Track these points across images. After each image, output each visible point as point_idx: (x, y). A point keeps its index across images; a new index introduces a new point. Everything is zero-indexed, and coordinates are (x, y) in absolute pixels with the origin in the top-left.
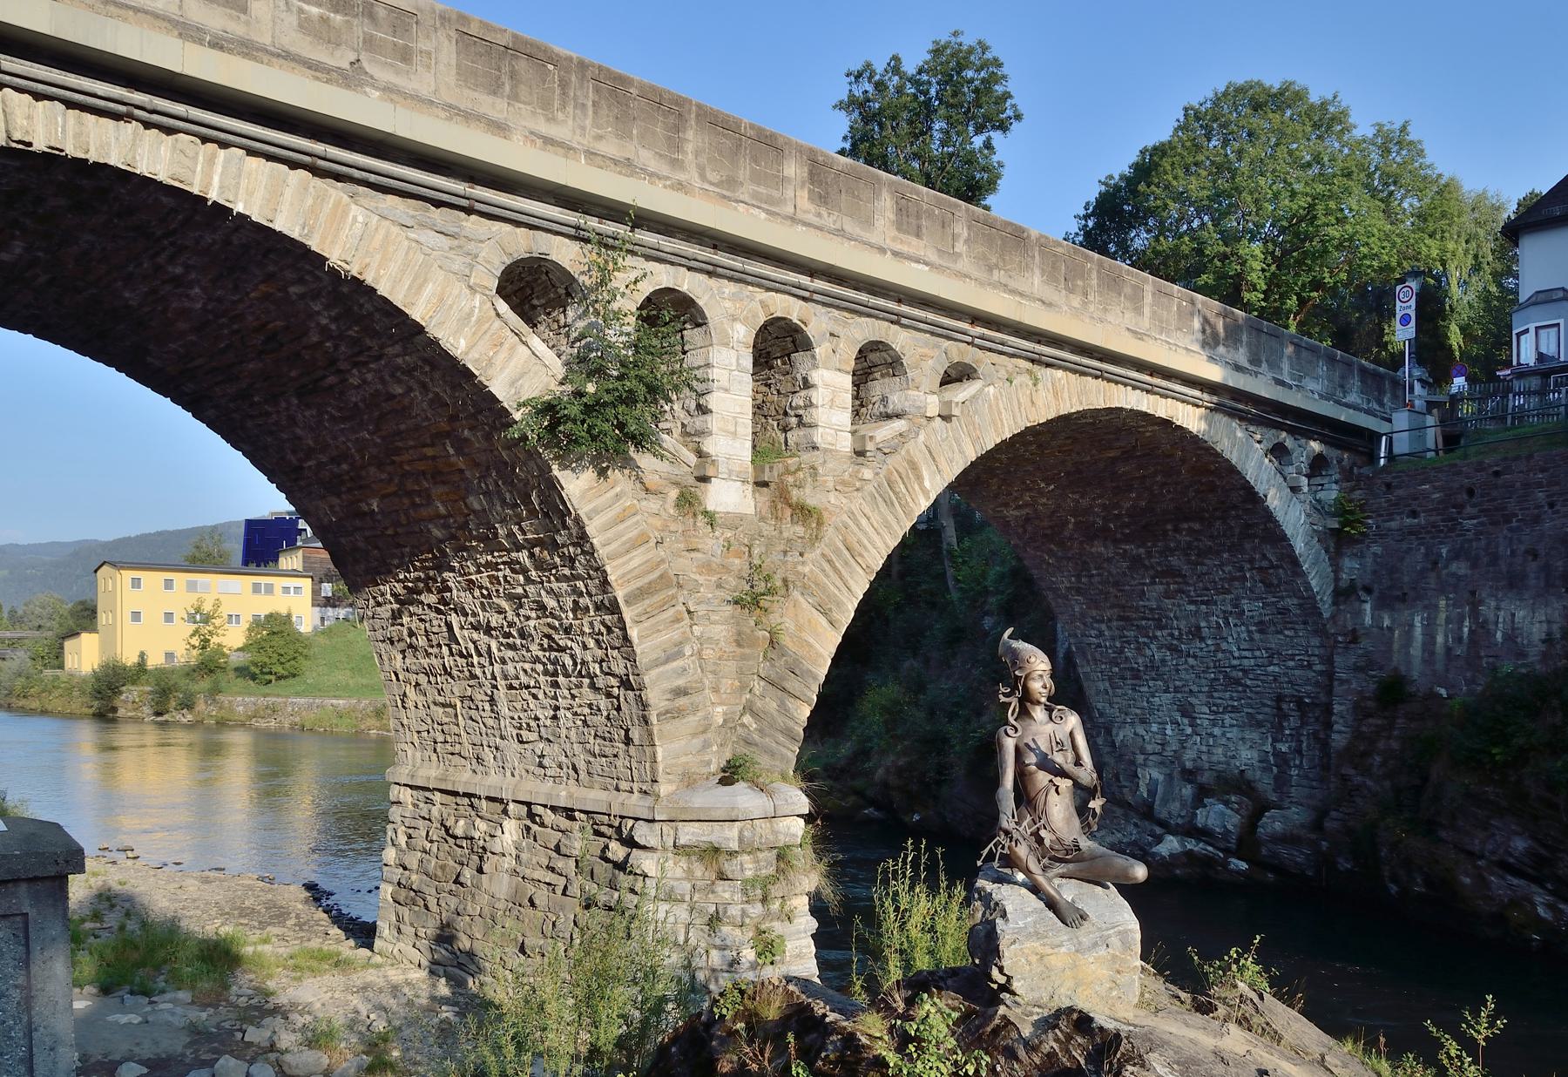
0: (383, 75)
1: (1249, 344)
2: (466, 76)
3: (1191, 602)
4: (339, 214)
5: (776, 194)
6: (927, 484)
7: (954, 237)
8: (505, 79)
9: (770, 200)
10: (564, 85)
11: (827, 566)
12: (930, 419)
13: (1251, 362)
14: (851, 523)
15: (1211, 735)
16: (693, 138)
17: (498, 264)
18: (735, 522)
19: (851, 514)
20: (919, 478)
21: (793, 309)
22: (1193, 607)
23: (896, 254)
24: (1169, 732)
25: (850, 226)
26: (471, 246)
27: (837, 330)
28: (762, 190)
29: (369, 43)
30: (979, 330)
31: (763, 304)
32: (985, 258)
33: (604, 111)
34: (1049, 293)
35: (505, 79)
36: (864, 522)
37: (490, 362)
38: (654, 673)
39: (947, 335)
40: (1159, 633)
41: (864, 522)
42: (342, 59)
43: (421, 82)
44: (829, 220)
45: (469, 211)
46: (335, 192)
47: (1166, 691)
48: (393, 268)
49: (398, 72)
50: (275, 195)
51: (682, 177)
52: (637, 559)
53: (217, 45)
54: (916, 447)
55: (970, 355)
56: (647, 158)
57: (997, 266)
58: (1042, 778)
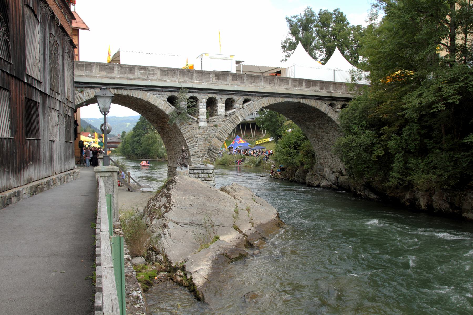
0: (150, 77)
1: (320, 86)
4: (146, 95)
5: (209, 80)
6: (240, 119)
7: (244, 80)
8: (167, 74)
9: (208, 81)
10: (175, 73)
11: (220, 133)
12: (240, 109)
13: (321, 89)
15: (336, 161)
17: (167, 97)
18: (204, 128)
19: (225, 125)
20: (238, 118)
21: (213, 96)
23: (231, 85)
25: (222, 82)
26: (163, 95)
27: (222, 97)
28: (207, 80)
29: (149, 74)
30: (250, 93)
31: (208, 96)
32: (251, 82)
33: (181, 75)
34: (265, 85)
35: (167, 74)
36: (227, 126)
37: (166, 110)
38: (191, 149)
39: (225, 94)
41: (227, 126)
42: (146, 77)
43: (155, 77)
45: (163, 91)
46: (146, 92)
48: (153, 100)
49: (152, 77)
50: (138, 95)
52: (188, 134)
53: (131, 79)
54: (237, 114)
55: (248, 97)
56: (188, 80)
57: (253, 83)
58: (72, 101)
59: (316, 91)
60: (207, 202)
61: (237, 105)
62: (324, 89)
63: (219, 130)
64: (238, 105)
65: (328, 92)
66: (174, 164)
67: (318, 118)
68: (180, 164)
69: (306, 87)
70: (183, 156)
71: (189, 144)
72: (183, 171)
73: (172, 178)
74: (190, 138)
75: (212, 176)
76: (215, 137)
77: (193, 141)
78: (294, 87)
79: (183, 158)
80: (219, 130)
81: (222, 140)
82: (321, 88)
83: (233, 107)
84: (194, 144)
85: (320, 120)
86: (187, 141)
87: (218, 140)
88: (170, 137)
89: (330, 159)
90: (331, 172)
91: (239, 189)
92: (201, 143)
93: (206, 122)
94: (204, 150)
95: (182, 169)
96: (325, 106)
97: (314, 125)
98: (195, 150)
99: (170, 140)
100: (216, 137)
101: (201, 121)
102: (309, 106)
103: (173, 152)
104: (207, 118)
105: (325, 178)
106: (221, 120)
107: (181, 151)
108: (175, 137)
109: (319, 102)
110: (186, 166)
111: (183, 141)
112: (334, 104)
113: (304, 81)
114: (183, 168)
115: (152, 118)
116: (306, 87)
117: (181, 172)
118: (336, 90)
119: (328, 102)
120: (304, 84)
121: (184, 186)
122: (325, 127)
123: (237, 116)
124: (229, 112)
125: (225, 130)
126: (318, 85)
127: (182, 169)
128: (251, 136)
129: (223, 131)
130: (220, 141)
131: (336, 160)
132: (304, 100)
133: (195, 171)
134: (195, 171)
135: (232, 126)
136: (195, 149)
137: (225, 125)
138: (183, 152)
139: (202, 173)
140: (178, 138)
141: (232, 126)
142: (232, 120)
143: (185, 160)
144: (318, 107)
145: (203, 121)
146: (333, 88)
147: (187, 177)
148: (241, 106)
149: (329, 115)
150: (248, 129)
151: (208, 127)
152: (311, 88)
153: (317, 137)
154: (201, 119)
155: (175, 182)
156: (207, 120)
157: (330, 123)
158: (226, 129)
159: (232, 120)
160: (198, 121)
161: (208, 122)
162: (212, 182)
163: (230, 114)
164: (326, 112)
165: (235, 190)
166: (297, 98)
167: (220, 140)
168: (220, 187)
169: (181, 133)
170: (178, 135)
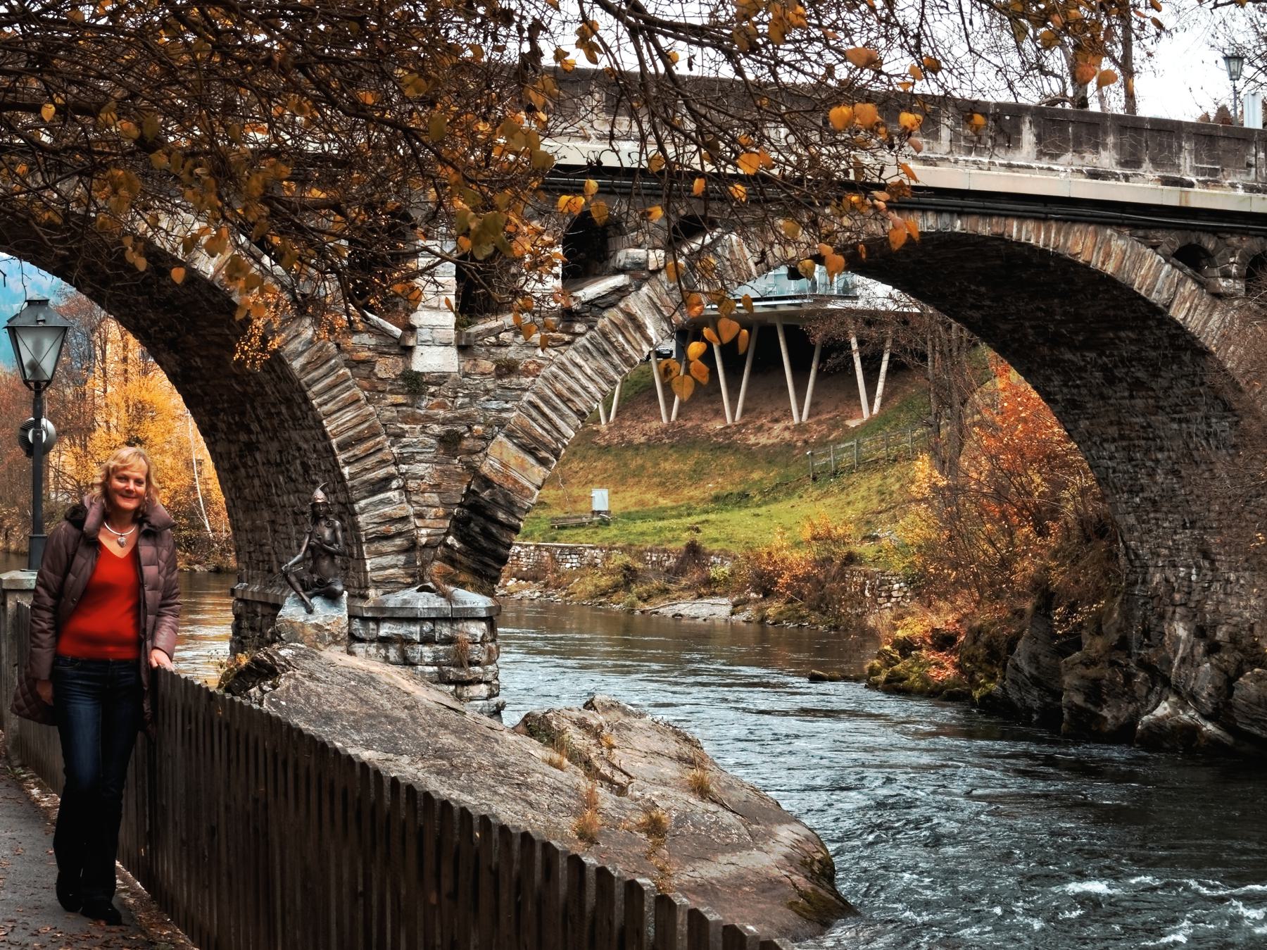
1: (1119, 147)
3: (1173, 420)
11: (534, 413)
13: (1123, 164)
14: (561, 374)
15: (1228, 581)
19: (562, 367)
20: (640, 328)
22: (1175, 426)
24: (1194, 578)
40: (1160, 456)
47: (1184, 527)
52: (348, 415)
59: (1094, 175)
60: (433, 777)
61: (632, 251)
62: (1147, 165)
63: (528, 396)
64: (639, 253)
65: (1166, 181)
66: (271, 584)
67: (1124, 329)
68: (302, 582)
69: (1041, 154)
70: (315, 541)
71: (353, 476)
72: (313, 620)
73: (261, 655)
74: (360, 440)
75: (484, 658)
76: (501, 437)
77: (379, 456)
78: (969, 152)
79: (318, 552)
80: (528, 396)
81: (543, 454)
82: (1131, 161)
83: (612, 264)
84: (381, 473)
85: (1132, 341)
86: (341, 457)
87: (522, 455)
88: (250, 432)
89: (1199, 568)
90: (1200, 649)
91: (619, 728)
92: (419, 469)
93: (453, 351)
94: (441, 512)
95: (310, 611)
96: (1153, 259)
97: (1104, 368)
98: (387, 510)
99: (251, 447)
100: (510, 435)
101: (424, 343)
102: (1058, 257)
103: (266, 515)
104: (458, 325)
105: (1166, 682)
106: (536, 338)
107: (307, 509)
108: (275, 430)
109: (1119, 244)
110: (332, 598)
111: (320, 457)
112: (1205, 251)
113: (1027, 119)
114: (317, 603)
115: (154, 322)
116: (1041, 154)
117: (303, 625)
118: (1214, 172)
119: (1172, 240)
120: (1028, 136)
121: (318, 695)
122: (1165, 384)
123: (632, 317)
124: (592, 290)
125: (559, 396)
126: (1111, 140)
127: (310, 611)
128: (787, 412)
129: (547, 401)
130: (531, 460)
131: (1232, 577)
132: (1030, 225)
133: (385, 630)
134: (385, 630)
135: (601, 373)
136: (389, 502)
137: (562, 367)
138: (316, 519)
139: (427, 640)
140: (295, 435)
141: (601, 373)
142: (605, 335)
143: (325, 563)
144: (1110, 269)
145: (432, 343)
146: (1198, 159)
147: (335, 655)
148: (656, 257)
149: (1178, 313)
150: (767, 365)
151: (466, 375)
152: (1068, 157)
153: (1122, 437)
154: (424, 334)
155: (277, 674)
156: (459, 336)
157: (1187, 357)
158: (570, 389)
159: (605, 335)
160: (411, 342)
161: (464, 349)
162: (483, 689)
163: (591, 303)
165: (595, 733)
166: (986, 214)
167: (531, 452)
168: (517, 719)
169: (312, 408)
170: (294, 418)
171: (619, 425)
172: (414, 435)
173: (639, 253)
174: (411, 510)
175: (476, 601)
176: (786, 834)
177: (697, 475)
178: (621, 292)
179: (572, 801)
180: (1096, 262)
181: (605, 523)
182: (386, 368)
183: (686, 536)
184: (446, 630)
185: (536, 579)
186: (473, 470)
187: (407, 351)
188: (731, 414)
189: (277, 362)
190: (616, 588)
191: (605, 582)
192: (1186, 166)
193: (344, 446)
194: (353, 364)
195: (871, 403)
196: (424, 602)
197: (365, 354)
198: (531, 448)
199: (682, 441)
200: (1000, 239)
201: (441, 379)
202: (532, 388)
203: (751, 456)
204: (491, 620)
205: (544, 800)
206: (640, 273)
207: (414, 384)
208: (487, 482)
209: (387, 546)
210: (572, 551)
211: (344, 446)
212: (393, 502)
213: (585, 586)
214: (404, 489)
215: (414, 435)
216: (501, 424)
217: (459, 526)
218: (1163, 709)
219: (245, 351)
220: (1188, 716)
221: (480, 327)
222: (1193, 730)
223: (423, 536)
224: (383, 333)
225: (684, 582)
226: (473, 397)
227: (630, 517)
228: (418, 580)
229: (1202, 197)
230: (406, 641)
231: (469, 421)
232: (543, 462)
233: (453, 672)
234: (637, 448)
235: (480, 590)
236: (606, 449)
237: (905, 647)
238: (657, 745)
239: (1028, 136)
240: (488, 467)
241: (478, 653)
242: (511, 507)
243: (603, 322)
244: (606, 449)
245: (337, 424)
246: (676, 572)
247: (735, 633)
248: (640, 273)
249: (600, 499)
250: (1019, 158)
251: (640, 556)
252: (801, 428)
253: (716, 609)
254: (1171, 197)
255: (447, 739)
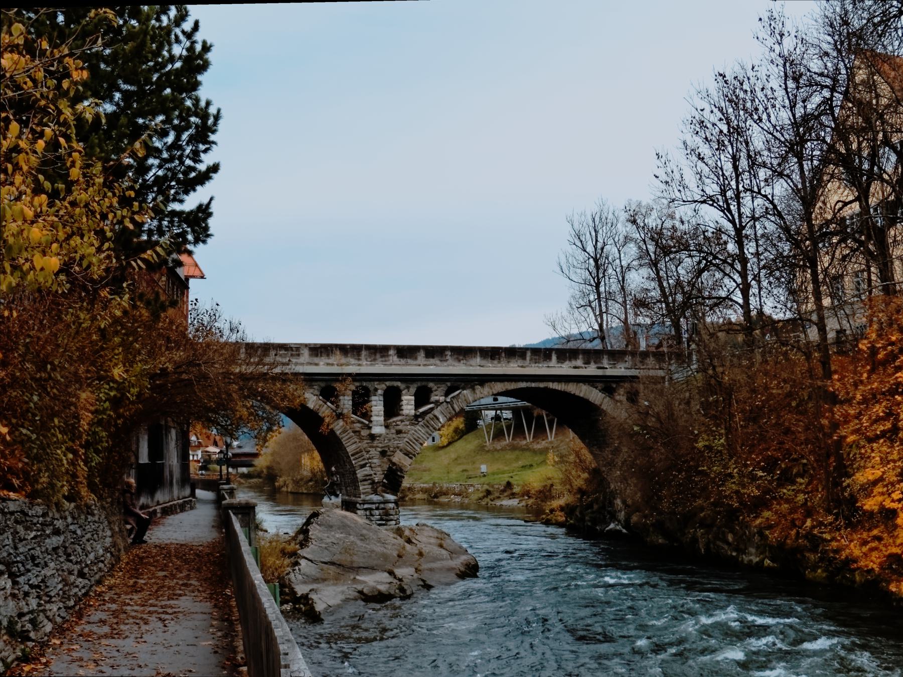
0: (294, 360)
1: (583, 359)
2: (311, 355)
13: (585, 363)
16: (364, 353)
20: (438, 419)
25: (409, 361)
29: (292, 355)
44: (403, 361)
51: (360, 362)
52: (354, 446)
56: (353, 361)
59: (575, 367)
62: (592, 363)
63: (406, 439)
65: (599, 368)
74: (357, 453)
82: (587, 362)
86: (352, 458)
110: (337, 496)
114: (333, 497)
116: (558, 362)
119: (600, 385)
120: (554, 357)
123: (435, 416)
124: (422, 410)
133: (366, 506)
134: (366, 506)
139: (377, 509)
144: (581, 395)
146: (609, 360)
148: (442, 399)
152: (567, 362)
154: (374, 423)
161: (387, 427)
162: (394, 522)
164: (597, 403)
171: (492, 444)
172: (373, 452)
173: (437, 398)
174: (372, 472)
175: (391, 497)
176: (464, 558)
177: (517, 459)
178: (432, 409)
179: (507, 578)
180: (577, 393)
181: (485, 476)
182: (364, 433)
183: (507, 479)
184: (382, 506)
185: (460, 495)
186: (390, 461)
187: (370, 428)
188: (529, 438)
189: (332, 432)
190: (484, 497)
191: (481, 495)
192: (605, 362)
193: (353, 455)
194: (354, 432)
195: (509, 436)
196: (375, 498)
197: (358, 429)
198: (407, 454)
199: (514, 448)
200: (546, 388)
201: (380, 436)
202: (406, 438)
203: (535, 452)
204: (396, 502)
205: (389, 547)
206: (437, 403)
207: (373, 437)
208: (394, 464)
209: (365, 483)
210: (472, 485)
211: (353, 455)
212: (367, 470)
213: (474, 497)
214: (370, 466)
215: (373, 452)
216: (398, 447)
217: (386, 476)
218: (612, 526)
219: (323, 429)
220: (619, 527)
221: (391, 420)
222: (620, 531)
223: (376, 480)
224: (362, 423)
225: (506, 494)
226: (390, 440)
227: (493, 474)
228: (375, 492)
229: (610, 372)
230: (371, 509)
231: (388, 447)
232: (411, 458)
233: (384, 517)
234: (498, 451)
235: (393, 494)
236: (488, 451)
237: (552, 511)
238: (431, 534)
239: (554, 357)
240: (395, 459)
241: (392, 512)
242: (401, 471)
243: (427, 417)
244: (488, 451)
245: (350, 449)
246: (503, 491)
247: (519, 510)
248: (437, 403)
249: (484, 468)
250: (551, 364)
251: (493, 487)
252: (551, 442)
253: (514, 502)
254: (600, 372)
255: (364, 532)
